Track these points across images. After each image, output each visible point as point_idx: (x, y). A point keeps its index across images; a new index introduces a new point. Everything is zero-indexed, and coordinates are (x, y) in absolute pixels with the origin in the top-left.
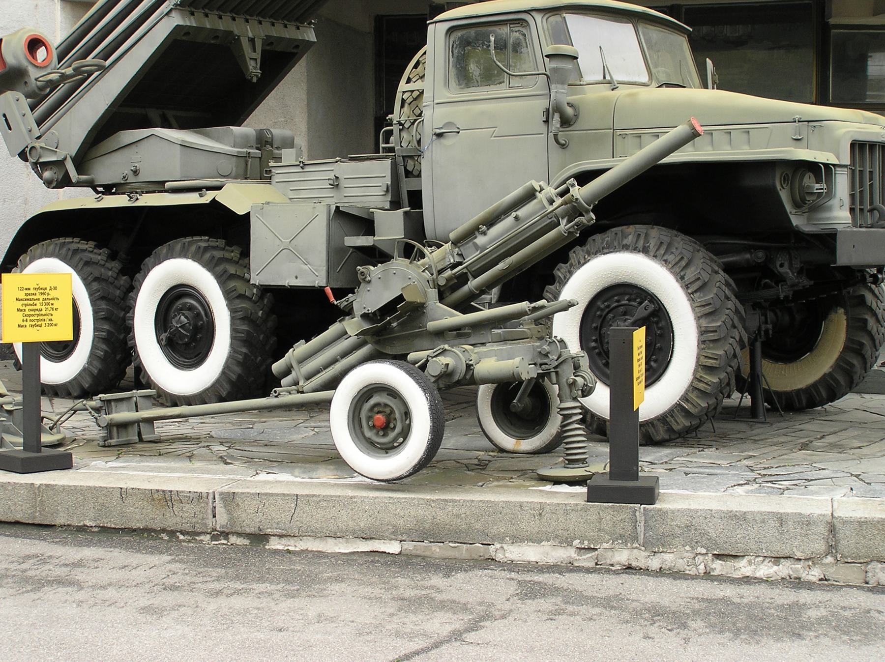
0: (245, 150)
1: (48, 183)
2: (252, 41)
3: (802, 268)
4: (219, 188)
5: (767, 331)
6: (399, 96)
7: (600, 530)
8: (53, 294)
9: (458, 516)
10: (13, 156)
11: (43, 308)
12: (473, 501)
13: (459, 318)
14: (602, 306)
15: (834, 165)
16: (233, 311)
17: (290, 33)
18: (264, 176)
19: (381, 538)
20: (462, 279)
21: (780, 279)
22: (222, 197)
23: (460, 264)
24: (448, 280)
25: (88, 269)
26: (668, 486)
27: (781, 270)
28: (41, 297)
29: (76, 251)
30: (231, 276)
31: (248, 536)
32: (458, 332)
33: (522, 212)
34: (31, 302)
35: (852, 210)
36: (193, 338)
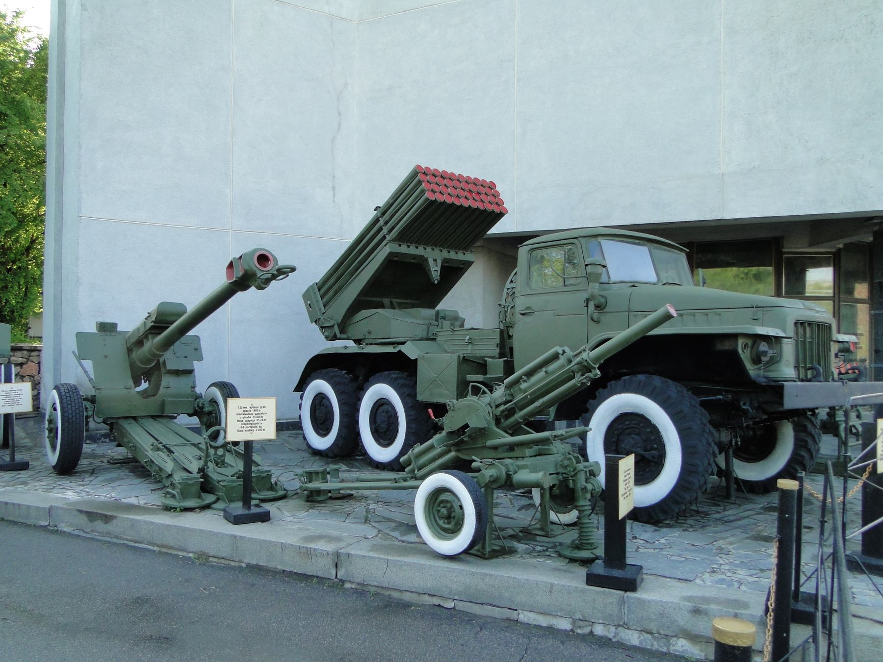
1: (327, 337)
2: (435, 260)
4: (403, 343)
5: (736, 442)
6: (505, 290)
7: (594, 608)
8: (263, 410)
9: (493, 586)
13: (509, 439)
17: (461, 256)
20: (511, 412)
22: (404, 349)
23: (511, 401)
24: (503, 411)
28: (254, 413)
30: (408, 393)
33: (552, 367)
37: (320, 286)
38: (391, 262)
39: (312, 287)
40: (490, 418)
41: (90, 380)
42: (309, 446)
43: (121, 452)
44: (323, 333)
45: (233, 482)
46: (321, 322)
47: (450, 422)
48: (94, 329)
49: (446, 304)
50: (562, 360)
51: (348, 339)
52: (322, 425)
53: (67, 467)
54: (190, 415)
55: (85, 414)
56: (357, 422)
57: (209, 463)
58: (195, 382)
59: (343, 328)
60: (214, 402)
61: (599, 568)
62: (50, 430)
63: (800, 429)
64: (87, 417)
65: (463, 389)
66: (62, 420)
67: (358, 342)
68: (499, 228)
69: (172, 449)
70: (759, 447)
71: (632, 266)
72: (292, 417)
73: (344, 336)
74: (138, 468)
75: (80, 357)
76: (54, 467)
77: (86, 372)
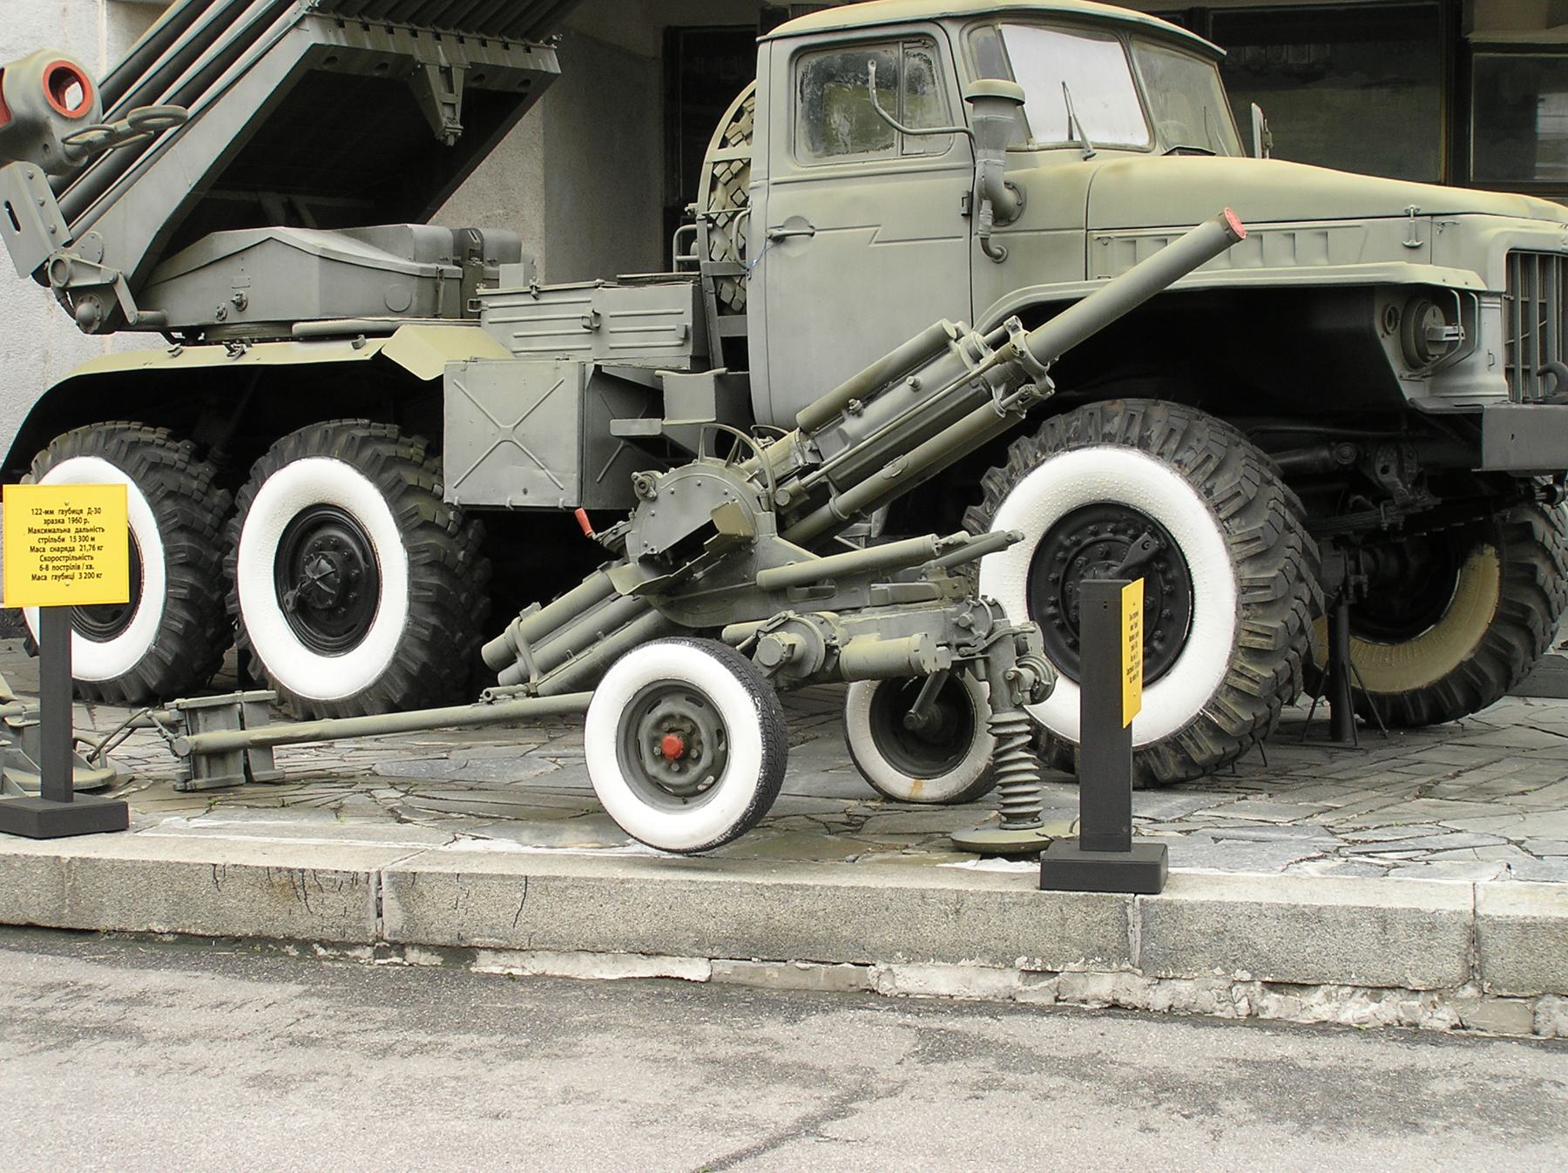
0: (433, 266)
1: (86, 325)
2: (446, 72)
3: (1420, 475)
4: (388, 333)
5: (1358, 587)
6: (706, 170)
7: (1062, 939)
8: (94, 521)
9: (812, 914)
10: (23, 276)
11: (77, 545)
12: (837, 888)
13: (814, 564)
14: (1067, 543)
15: (1478, 293)
16: (413, 551)
17: (514, 58)
18: (469, 312)
19: (675, 953)
20: (819, 495)
21: (1381, 495)
22: (393, 349)
23: (815, 467)
24: (794, 496)
25: (157, 477)
26: (1184, 862)
27: (1385, 478)
28: (73, 527)
29: (134, 445)
30: (410, 489)
31: (439, 949)
32: (812, 589)
33: (924, 376)
34: (55, 536)
35: (1509, 372)
36: (342, 600)
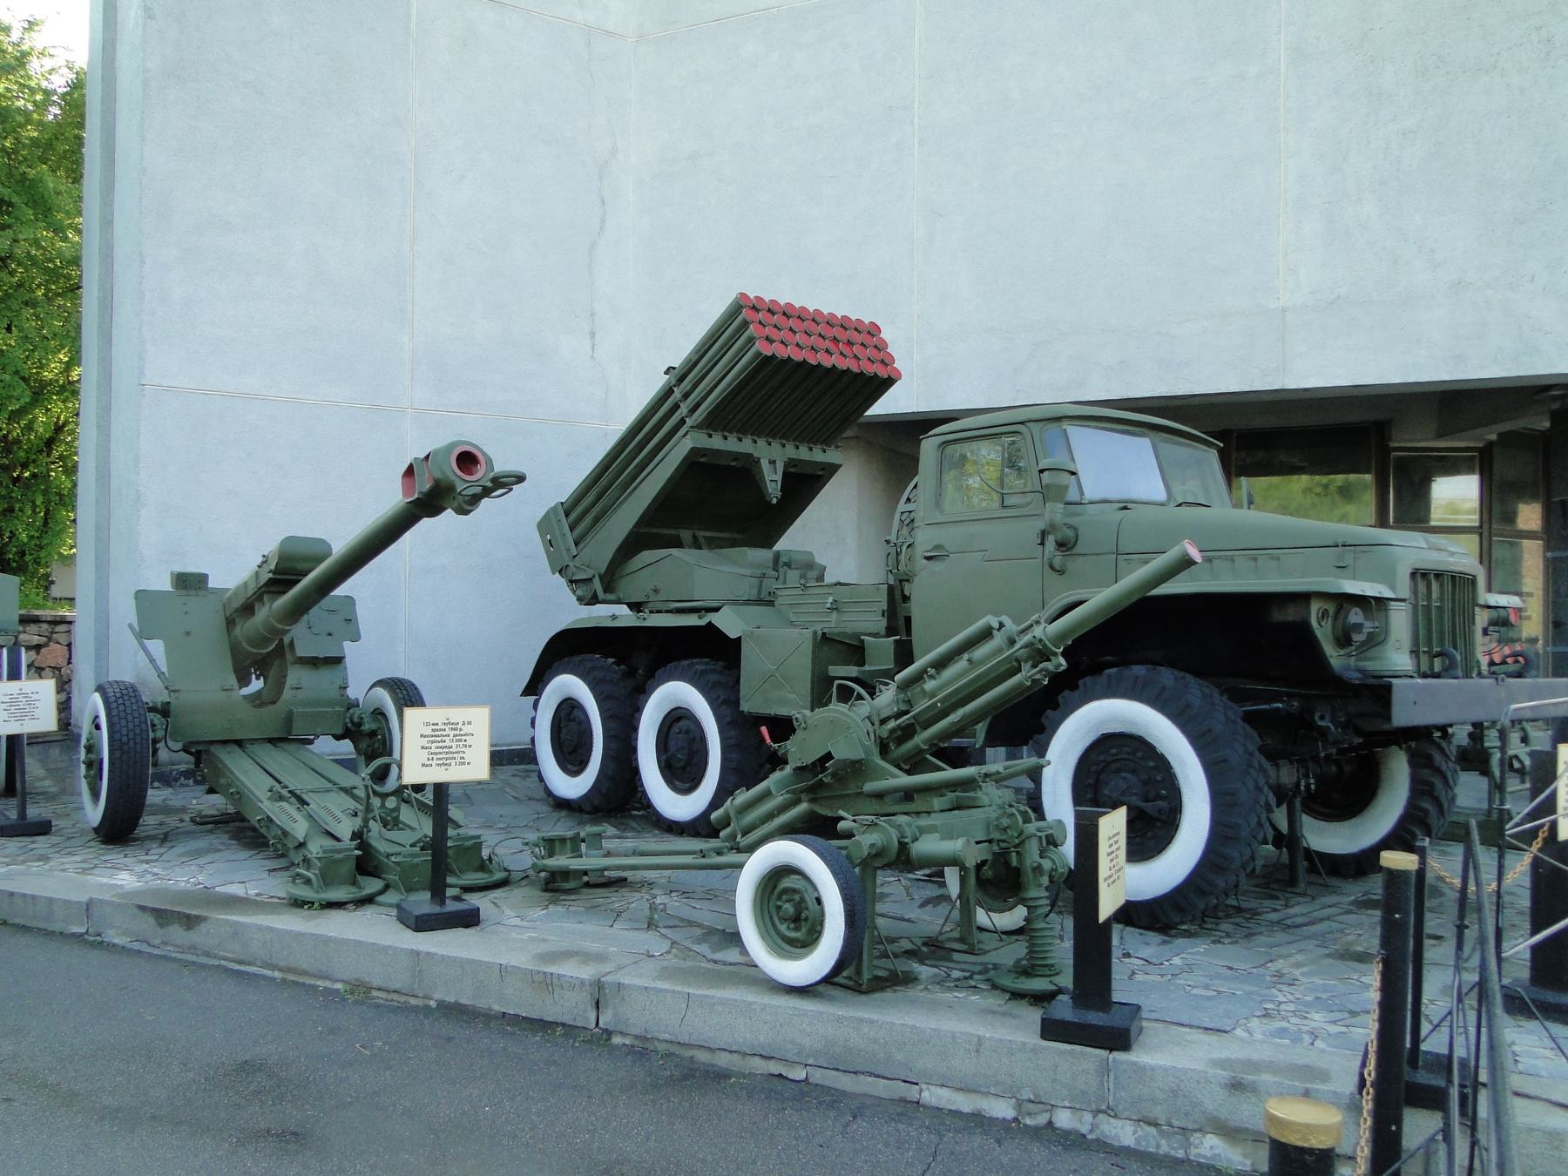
1: (580, 599)
2: (773, 462)
4: (716, 610)
5: (1308, 786)
6: (897, 516)
7: (1054, 1081)
8: (466, 729)
9: (875, 1041)
13: (904, 780)
17: (818, 455)
20: (907, 732)
22: (717, 619)
23: (907, 712)
24: (893, 731)
28: (452, 733)
30: (725, 697)
33: (980, 652)
37: (568, 508)
38: (695, 465)
39: (554, 509)
40: (870, 743)
41: (161, 674)
42: (549, 793)
43: (215, 803)
44: (574, 592)
45: (414, 855)
46: (569, 572)
47: (800, 750)
48: (166, 585)
49: (791, 541)
50: (998, 639)
51: (619, 602)
52: (572, 755)
53: (119, 829)
54: (338, 738)
55: (151, 735)
56: (634, 750)
57: (372, 823)
58: (346, 678)
59: (609, 583)
60: (379, 714)
61: (1063, 1009)
62: (89, 765)
63: (1420, 762)
64: (155, 741)
65: (822, 690)
66: (110, 745)
67: (636, 607)
68: (886, 406)
69: (305, 797)
70: (1348, 795)
71: (1122, 473)
72: (518, 740)
73: (610, 597)
74: (245, 831)
75: (142, 634)
76: (96, 830)
77: (152, 661)
